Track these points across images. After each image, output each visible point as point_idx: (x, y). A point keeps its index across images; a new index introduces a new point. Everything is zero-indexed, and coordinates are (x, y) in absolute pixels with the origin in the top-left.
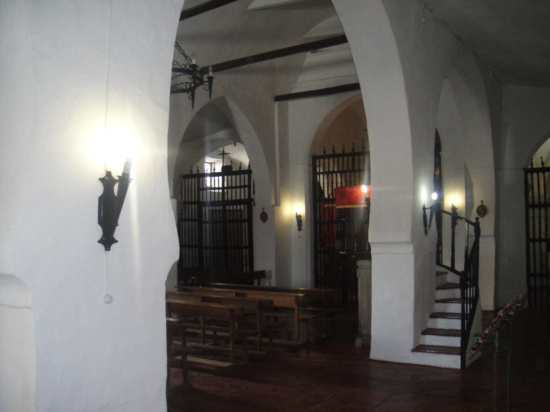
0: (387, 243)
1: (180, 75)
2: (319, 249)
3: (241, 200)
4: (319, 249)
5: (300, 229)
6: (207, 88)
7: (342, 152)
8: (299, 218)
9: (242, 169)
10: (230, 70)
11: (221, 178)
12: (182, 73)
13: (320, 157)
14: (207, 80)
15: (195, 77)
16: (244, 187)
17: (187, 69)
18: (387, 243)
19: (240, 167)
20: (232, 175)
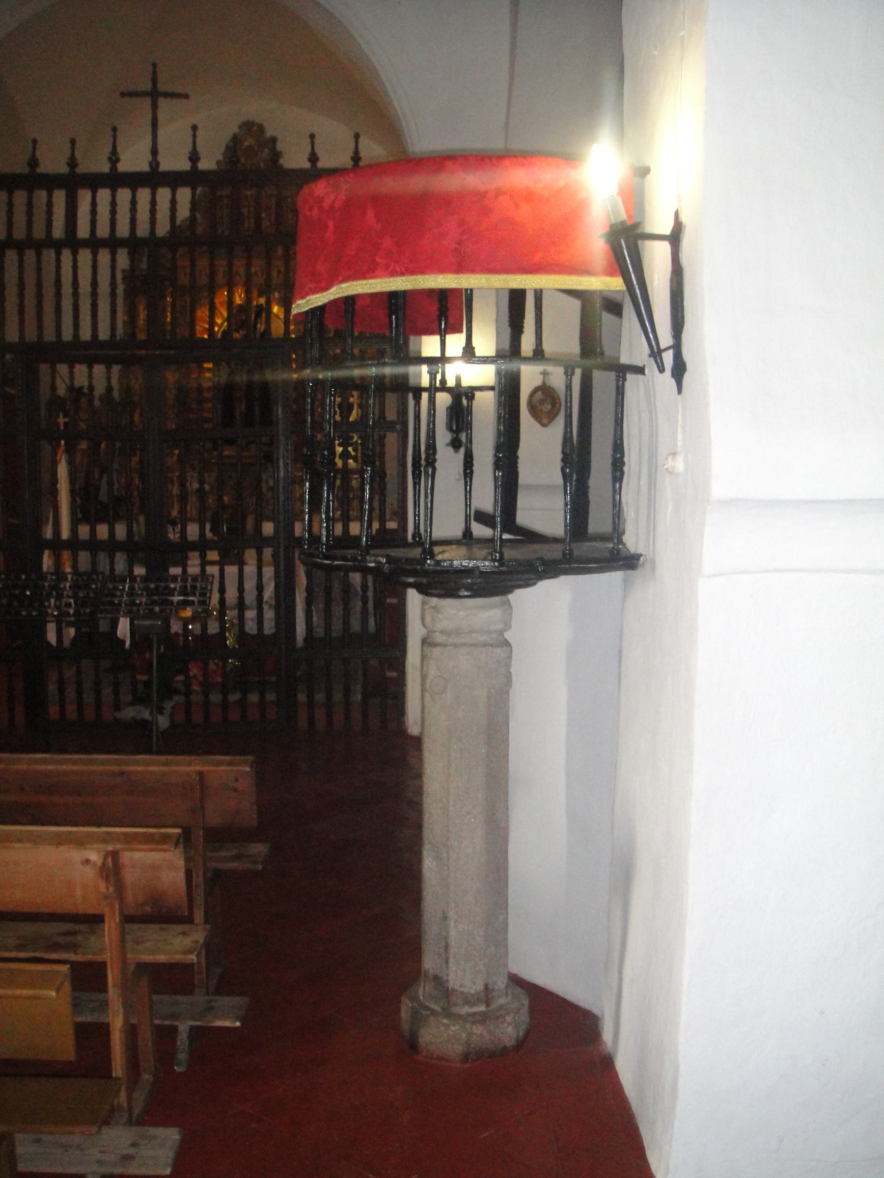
2: (65, 534)
4: (65, 534)
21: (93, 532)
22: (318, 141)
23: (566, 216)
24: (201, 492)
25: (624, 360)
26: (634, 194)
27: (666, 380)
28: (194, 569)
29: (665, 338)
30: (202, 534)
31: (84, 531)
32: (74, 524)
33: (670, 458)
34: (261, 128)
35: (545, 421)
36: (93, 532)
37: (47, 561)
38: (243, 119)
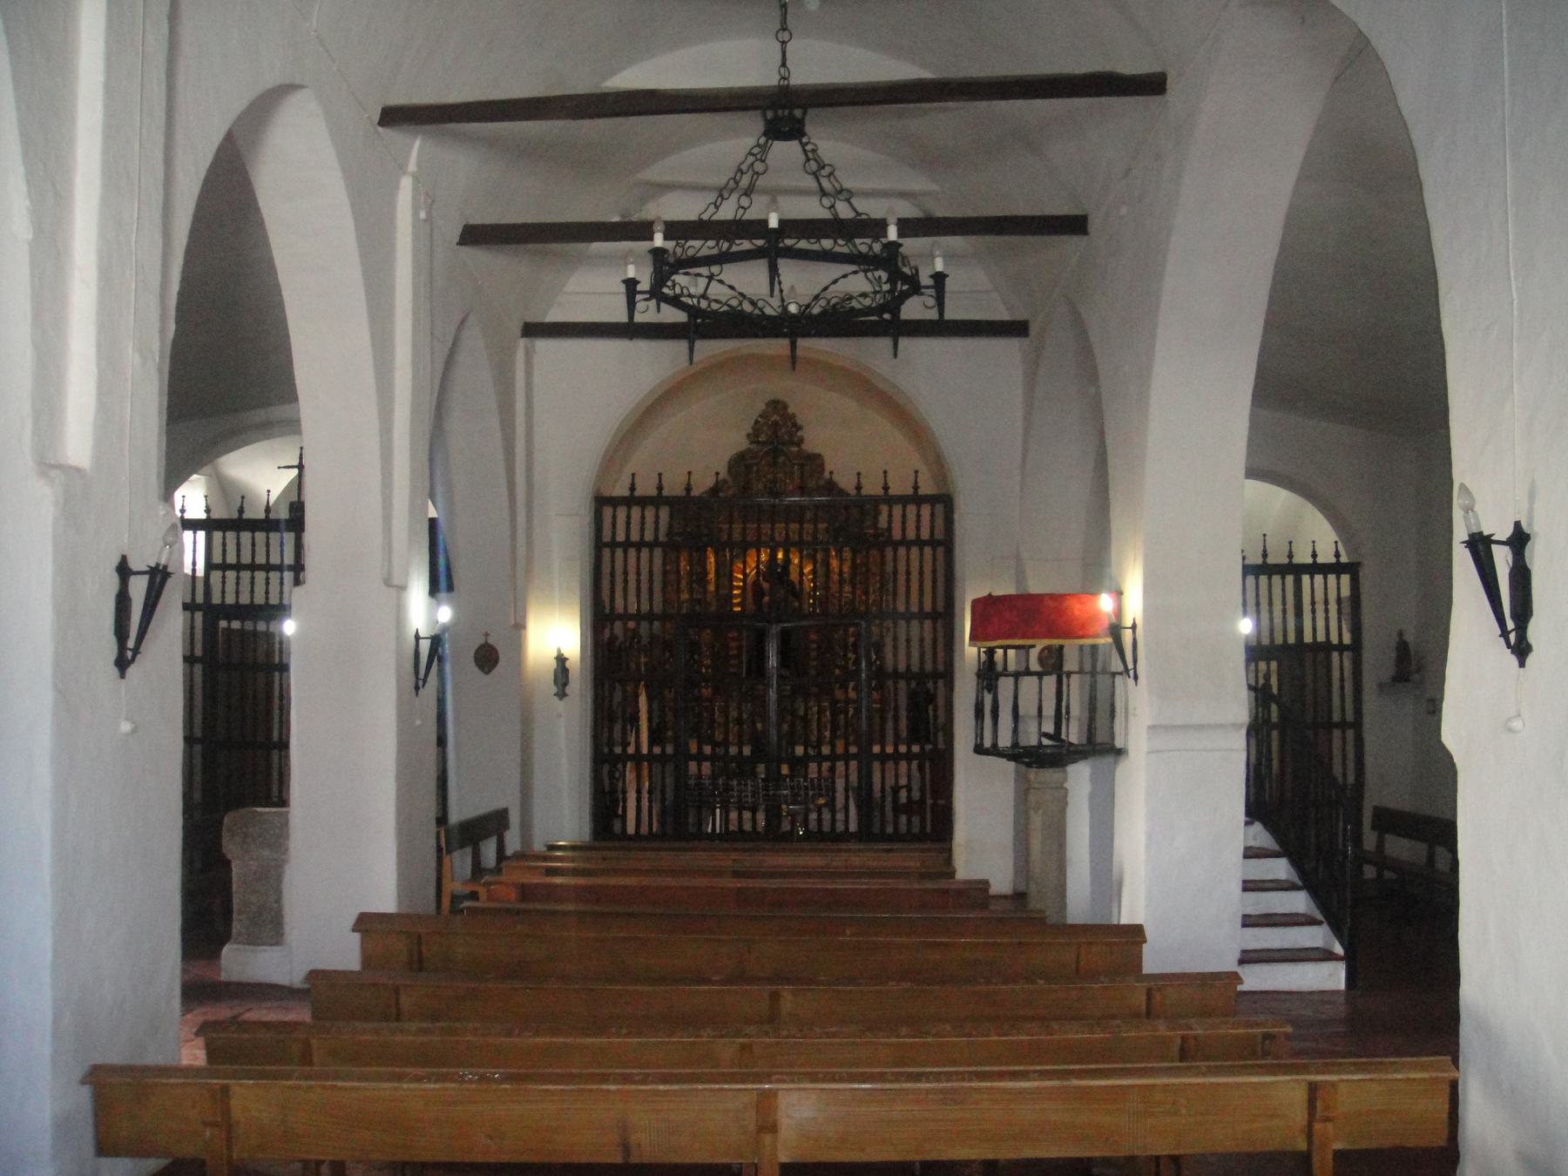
0: (1200, 727)
1: (855, 272)
2: (645, 751)
3: (237, 606)
4: (645, 751)
5: (562, 695)
6: (931, 302)
7: (880, 492)
8: (561, 659)
9: (245, 516)
10: (522, 247)
11: (201, 535)
12: (854, 268)
13: (614, 502)
14: (930, 282)
15: (895, 275)
16: (933, 543)
17: (876, 256)
18: (1200, 727)
19: (241, 510)
20: (253, 531)
21: (663, 750)
22: (890, 476)
23: (1096, 616)
24: (739, 721)
25: (1113, 670)
26: (1119, 612)
27: (1131, 681)
28: (813, 774)
29: (1130, 666)
30: (699, 766)
31: (657, 750)
32: (651, 744)
33: (767, 1139)
34: (785, 407)
35: (622, 524)
36: (663, 750)
37: (693, 766)
38: (769, 397)
